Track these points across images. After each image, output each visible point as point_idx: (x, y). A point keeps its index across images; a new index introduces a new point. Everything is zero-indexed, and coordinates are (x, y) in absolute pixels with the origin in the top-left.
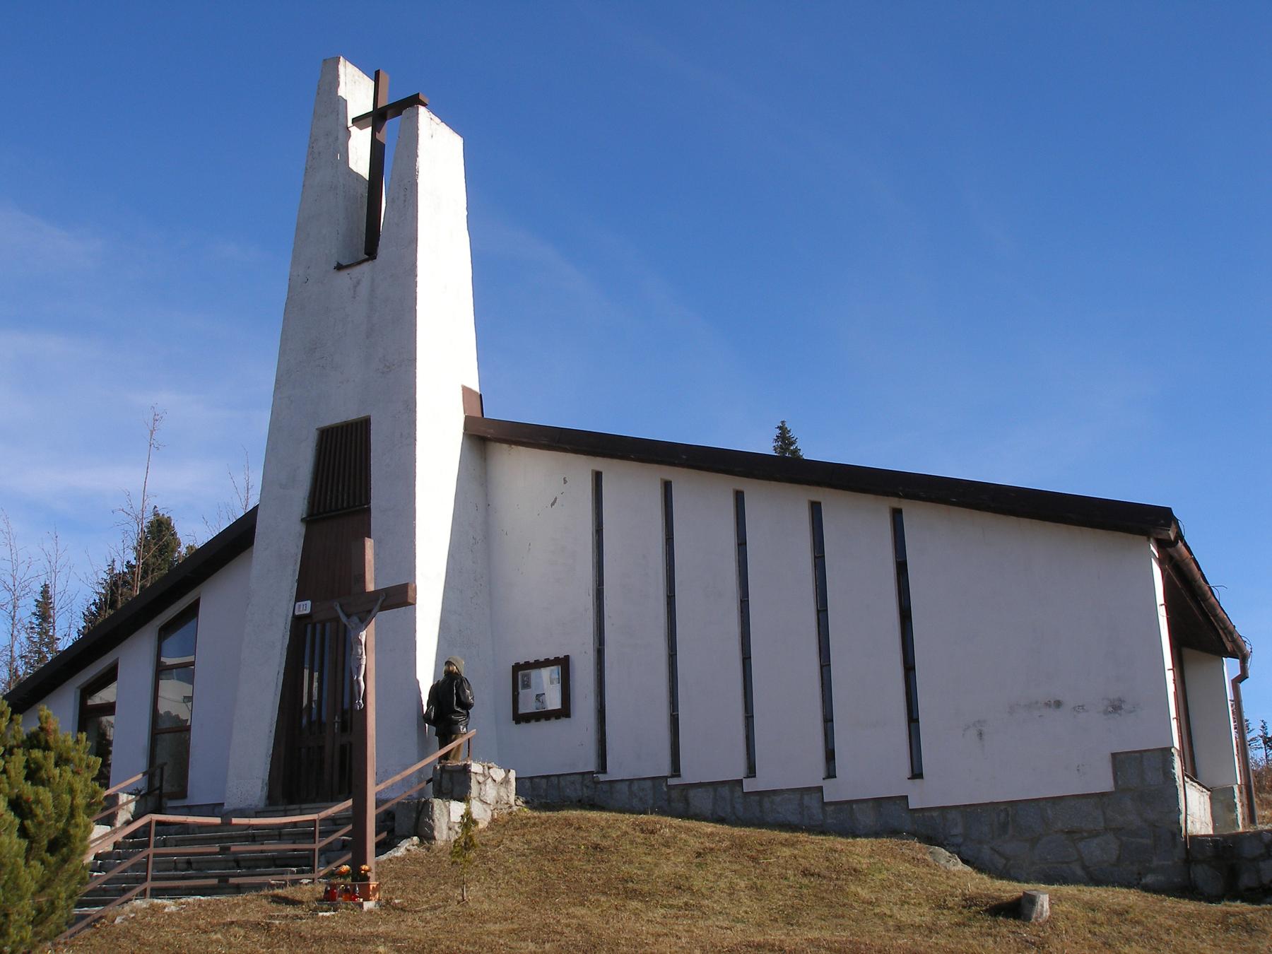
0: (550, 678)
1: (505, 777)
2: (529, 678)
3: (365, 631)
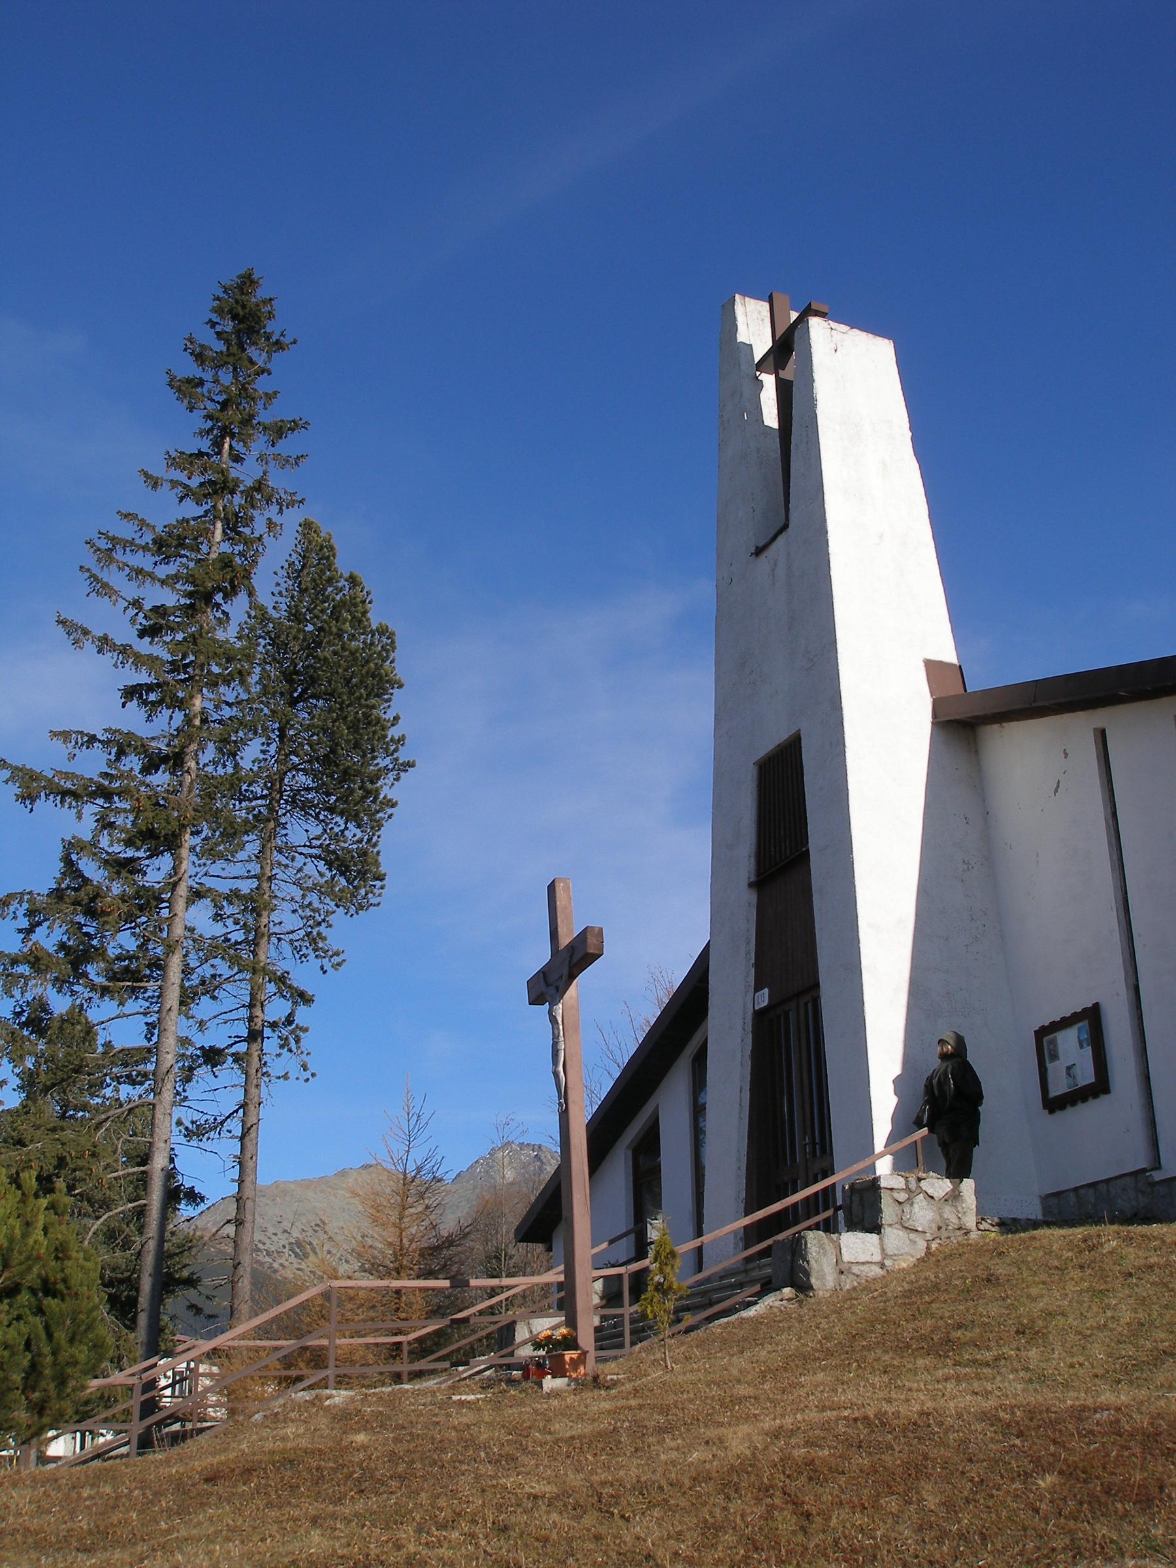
0: (1079, 1038)
1: (953, 1190)
2: (1055, 1046)
3: (560, 1005)
